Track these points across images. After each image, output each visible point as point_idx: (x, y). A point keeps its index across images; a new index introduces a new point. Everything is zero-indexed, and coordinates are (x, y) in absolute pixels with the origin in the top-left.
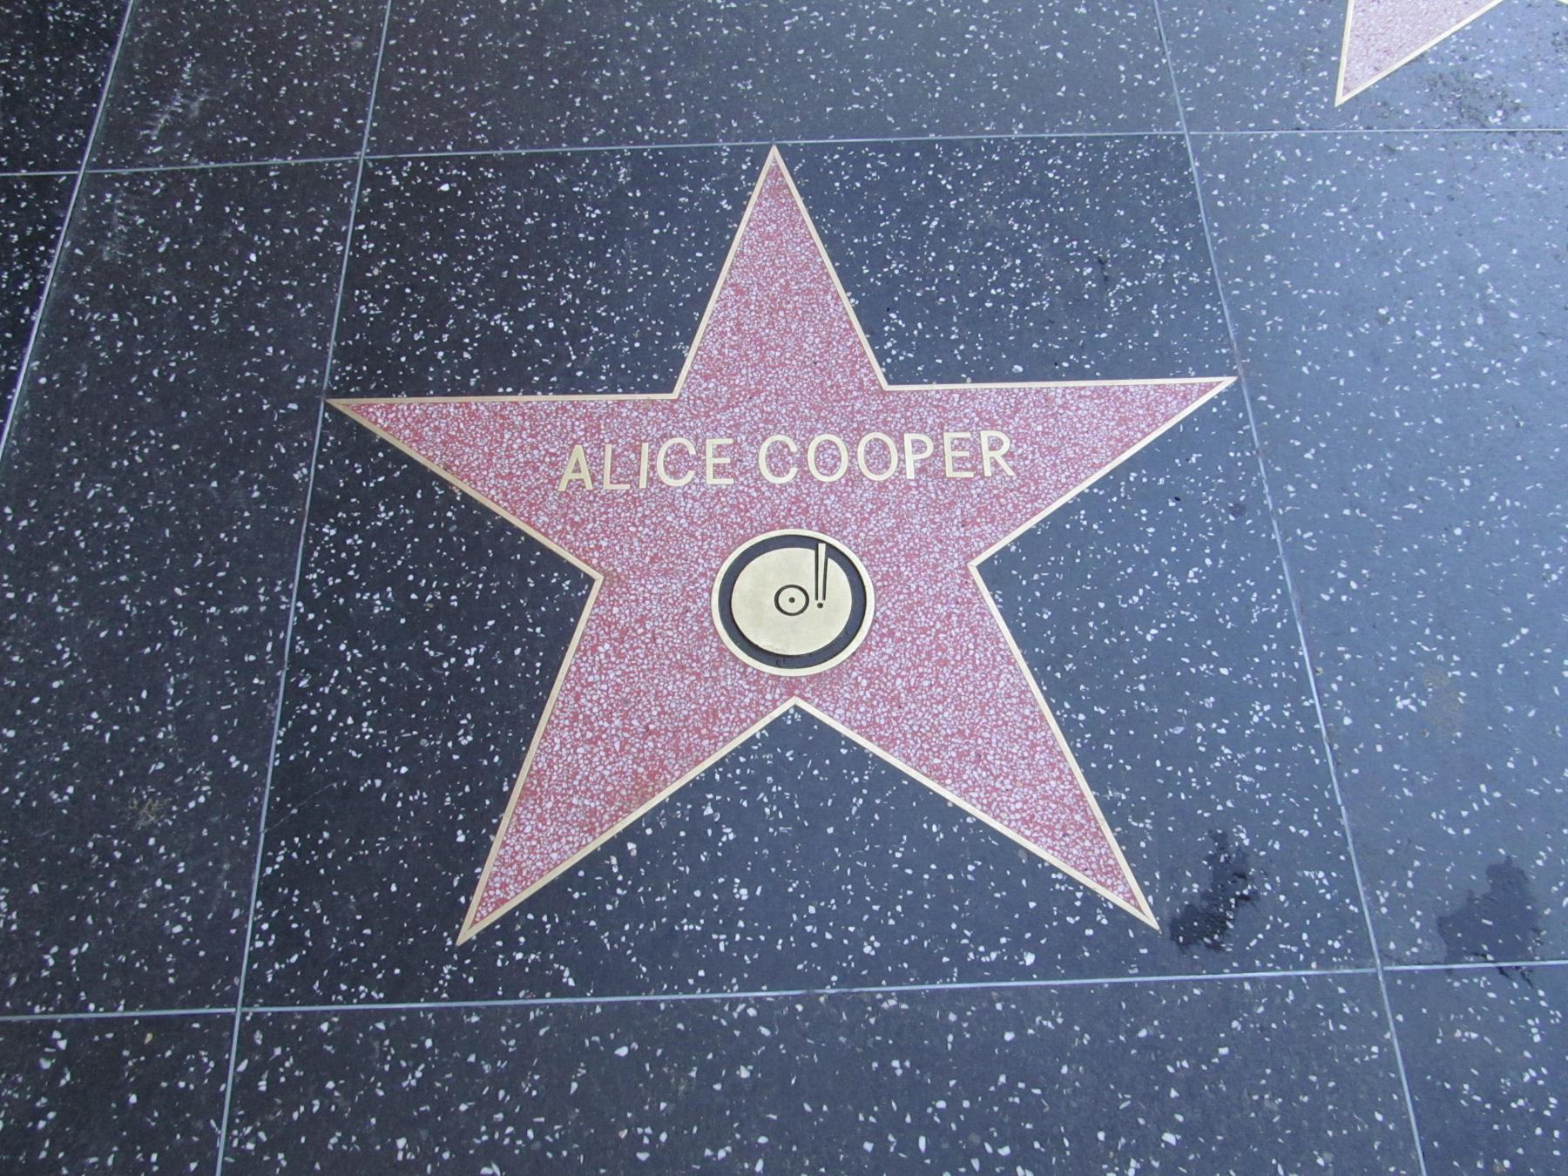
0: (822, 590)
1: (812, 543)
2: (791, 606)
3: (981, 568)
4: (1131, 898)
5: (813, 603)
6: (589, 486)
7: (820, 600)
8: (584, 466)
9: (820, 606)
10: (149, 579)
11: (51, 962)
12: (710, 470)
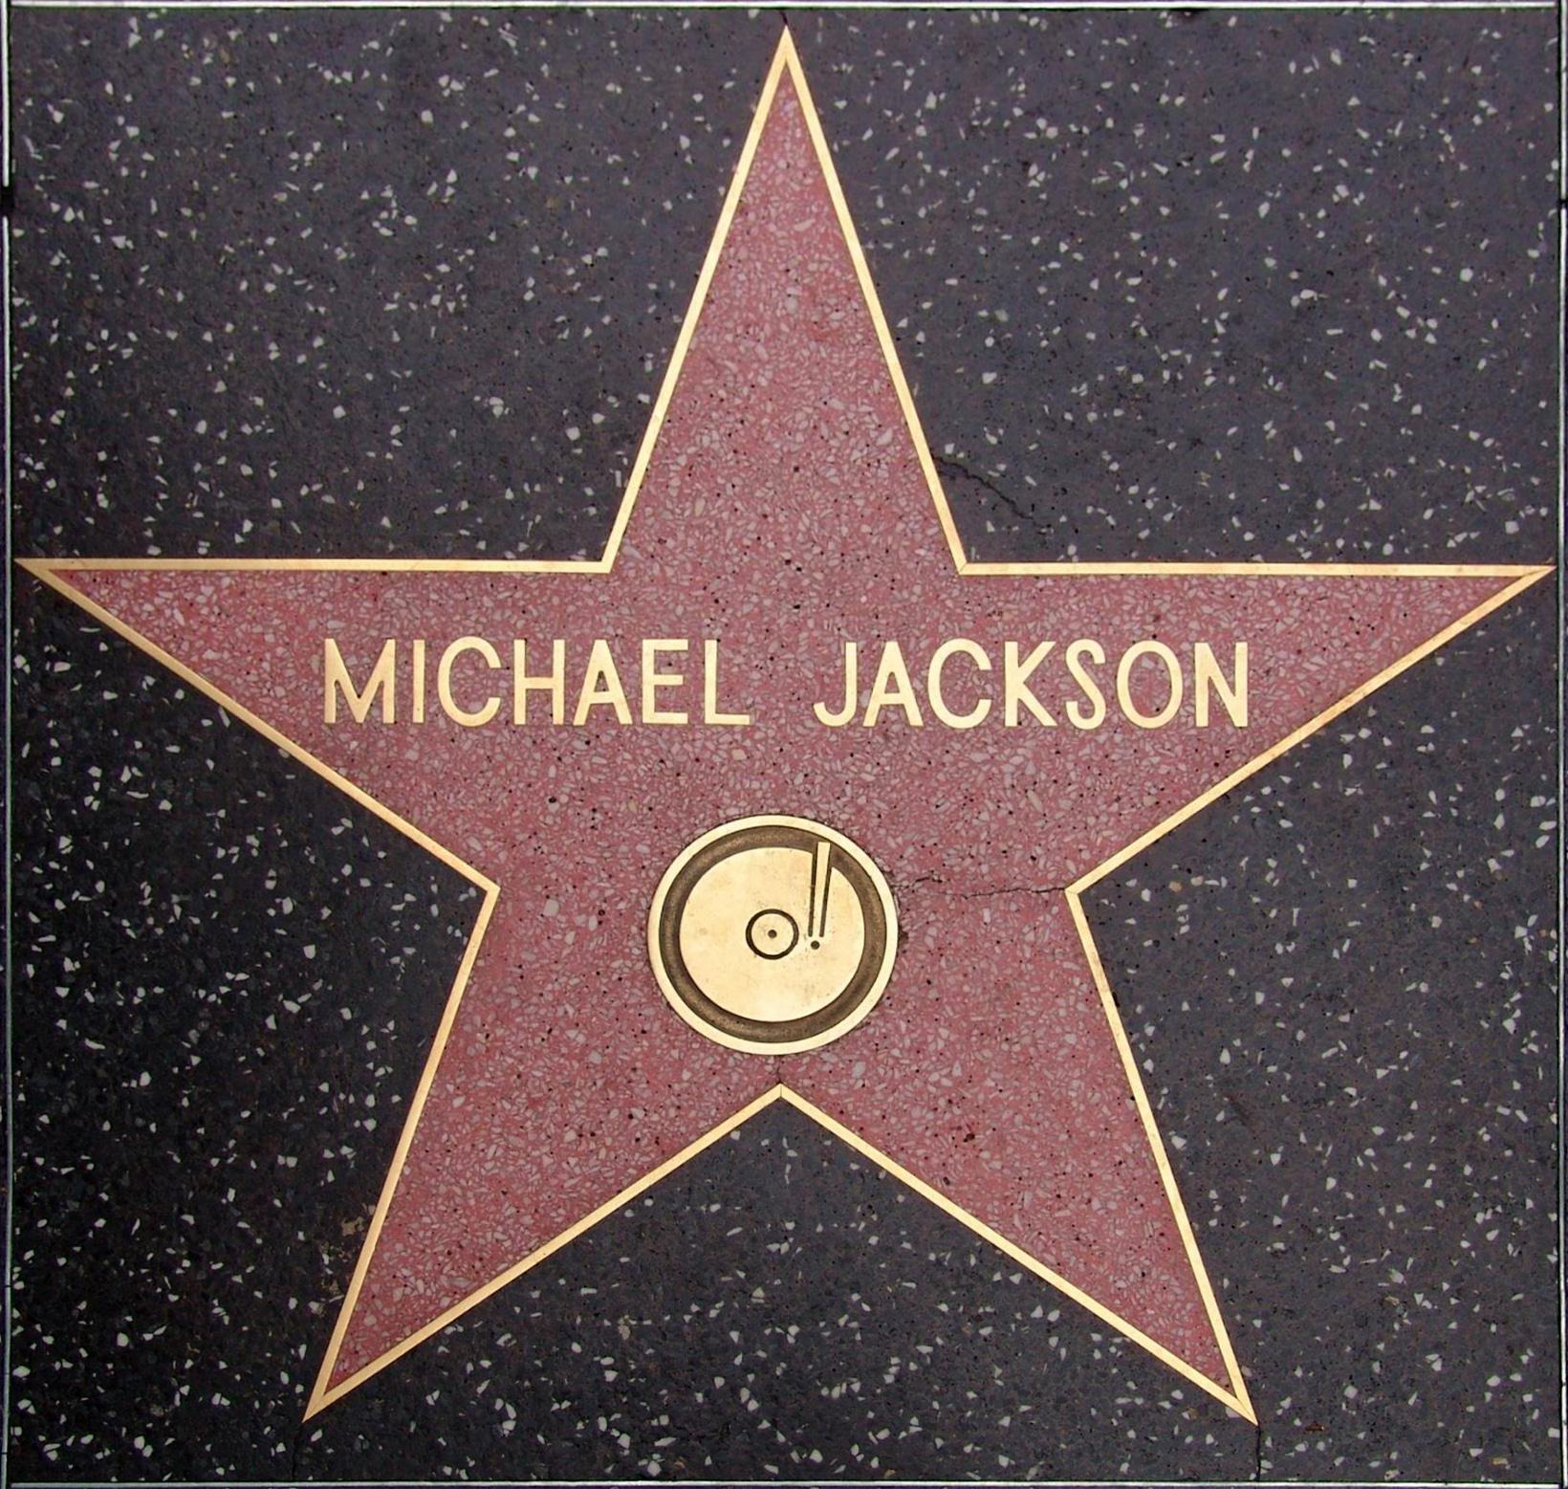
0: (818, 920)
1: (808, 842)
2: (768, 941)
5: (804, 943)
7: (816, 937)
9: (815, 945)
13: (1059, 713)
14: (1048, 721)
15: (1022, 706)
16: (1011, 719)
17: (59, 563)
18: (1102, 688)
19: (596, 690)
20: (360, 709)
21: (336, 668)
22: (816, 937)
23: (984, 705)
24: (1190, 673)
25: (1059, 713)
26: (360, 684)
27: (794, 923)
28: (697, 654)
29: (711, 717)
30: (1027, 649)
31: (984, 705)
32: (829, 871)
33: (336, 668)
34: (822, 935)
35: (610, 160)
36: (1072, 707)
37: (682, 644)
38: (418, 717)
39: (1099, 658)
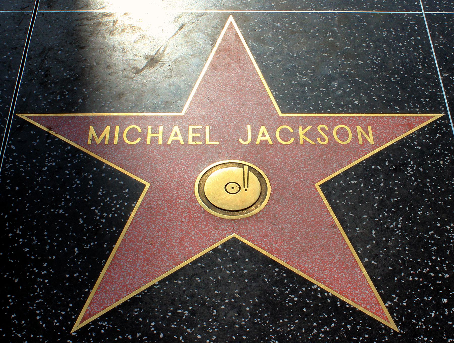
0: (246, 182)
1: (243, 166)
5: (243, 189)
7: (246, 188)
9: (246, 190)
11: (89, 245)
13: (315, 141)
15: (304, 140)
16: (302, 143)
18: (252, 136)
19: (262, 136)
20: (98, 141)
22: (246, 188)
25: (315, 141)
26: (99, 136)
27: (228, 192)
28: (204, 129)
29: (208, 142)
32: (248, 173)
34: (248, 187)
35: (405, 304)
36: (319, 139)
37: (201, 127)
38: (116, 142)
39: (327, 128)
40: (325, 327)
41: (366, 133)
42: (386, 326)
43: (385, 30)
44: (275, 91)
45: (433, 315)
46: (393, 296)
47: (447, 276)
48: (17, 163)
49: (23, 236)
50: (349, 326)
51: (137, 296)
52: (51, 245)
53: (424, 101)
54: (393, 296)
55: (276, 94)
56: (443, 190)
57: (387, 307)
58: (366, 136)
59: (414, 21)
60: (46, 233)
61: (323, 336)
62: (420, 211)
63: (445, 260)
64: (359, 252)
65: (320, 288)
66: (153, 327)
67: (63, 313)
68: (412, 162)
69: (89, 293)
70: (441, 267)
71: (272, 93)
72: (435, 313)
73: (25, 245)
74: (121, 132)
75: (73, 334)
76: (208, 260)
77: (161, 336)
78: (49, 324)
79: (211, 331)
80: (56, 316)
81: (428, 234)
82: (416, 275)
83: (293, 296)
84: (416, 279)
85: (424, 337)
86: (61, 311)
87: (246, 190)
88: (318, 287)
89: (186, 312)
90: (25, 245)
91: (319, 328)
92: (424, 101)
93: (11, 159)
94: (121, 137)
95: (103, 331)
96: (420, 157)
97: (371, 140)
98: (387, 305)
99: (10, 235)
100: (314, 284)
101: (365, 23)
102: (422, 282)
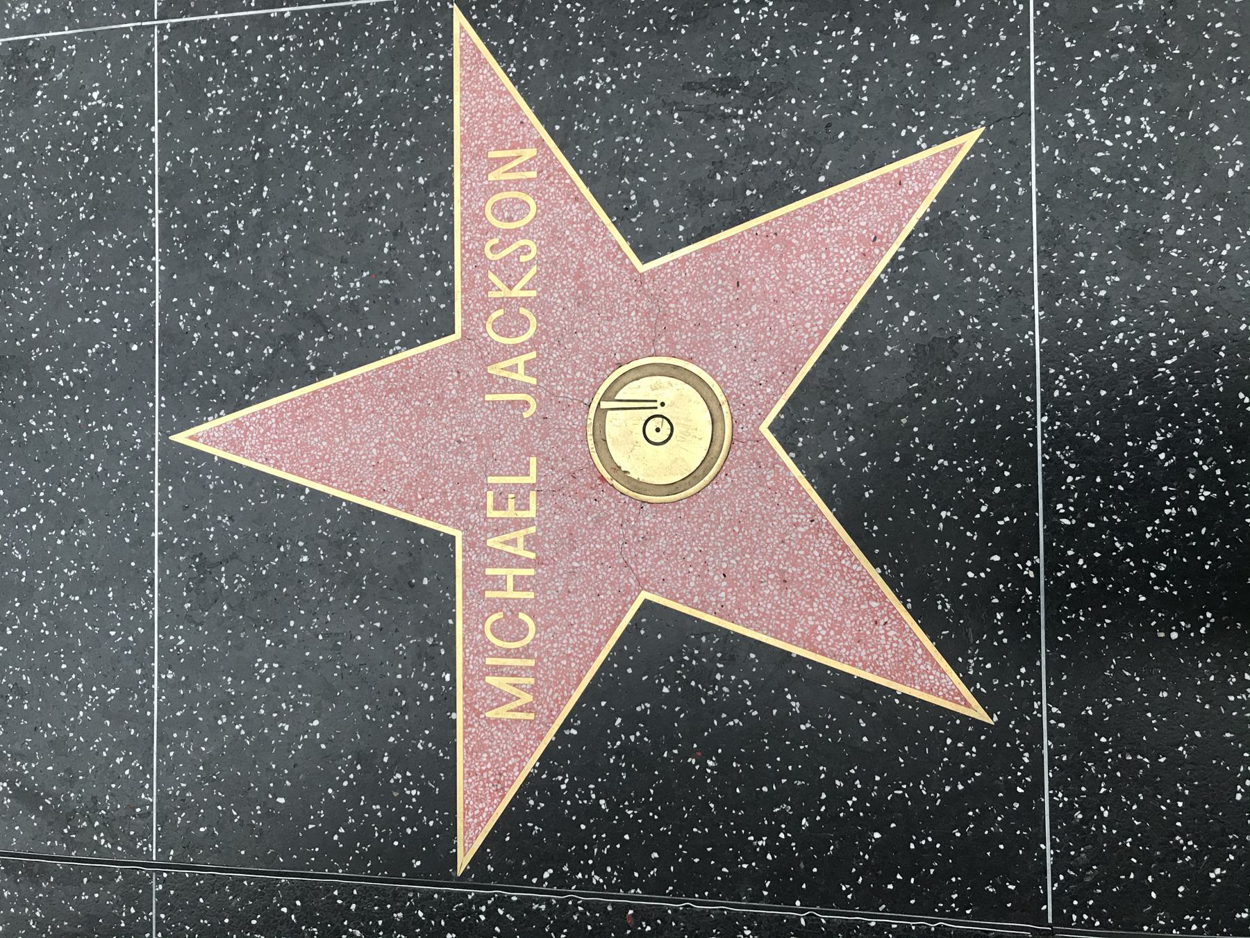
1: (601, 413)
2: (664, 431)
3: (644, 260)
4: (935, 166)
6: (532, 530)
8: (507, 537)
9: (663, 404)
10: (687, 859)
11: (793, 704)
12: (521, 514)
14: (534, 269)
17: (502, 169)
18: (516, 391)
20: (527, 698)
21: (502, 713)
23: (523, 311)
24: (509, 175)
25: (531, 263)
26: (510, 698)
28: (493, 486)
29: (532, 479)
30: (490, 287)
31: (523, 311)
33: (502, 713)
36: (523, 259)
39: (495, 241)
40: (975, 260)
41: (505, 163)
42: (972, 151)
43: (211, 110)
44: (392, 346)
45: (946, 63)
46: (903, 133)
47: (857, 30)
48: (590, 862)
49: (772, 833)
50: (973, 218)
51: (909, 606)
52: (796, 775)
53: (418, 41)
54: (903, 133)
55: (399, 344)
56: (651, 21)
57: (929, 147)
58: (515, 163)
59: (183, 45)
60: (765, 789)
61: (993, 266)
62: (705, 71)
63: (822, 31)
64: (803, 192)
65: (887, 267)
66: (977, 574)
67: (949, 741)
68: (582, 79)
69: (904, 697)
70: (838, 40)
71: (396, 353)
72: (943, 59)
73: (794, 825)
74: (508, 653)
75: (996, 718)
76: (821, 476)
77: (996, 558)
78: (973, 765)
79: (984, 469)
80: (956, 754)
81: (760, 60)
82: (857, 89)
83: (906, 319)
84: (864, 88)
85: (995, 83)
86: (946, 745)
87: (663, 404)
88: (884, 271)
89: (943, 514)
90: (794, 825)
91: (976, 274)
92: (418, 41)
93: (580, 875)
94: (517, 654)
95: (989, 666)
96: (568, 61)
97: (530, 152)
98: (924, 146)
99: (769, 857)
100: (879, 280)
101: (192, 151)
102: (872, 78)
